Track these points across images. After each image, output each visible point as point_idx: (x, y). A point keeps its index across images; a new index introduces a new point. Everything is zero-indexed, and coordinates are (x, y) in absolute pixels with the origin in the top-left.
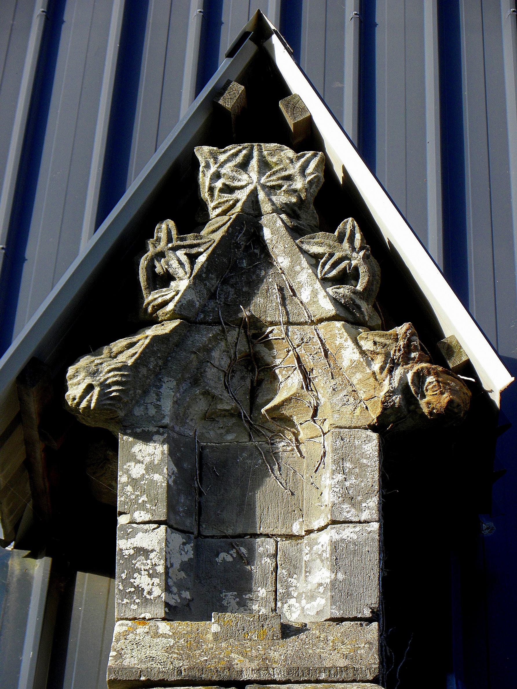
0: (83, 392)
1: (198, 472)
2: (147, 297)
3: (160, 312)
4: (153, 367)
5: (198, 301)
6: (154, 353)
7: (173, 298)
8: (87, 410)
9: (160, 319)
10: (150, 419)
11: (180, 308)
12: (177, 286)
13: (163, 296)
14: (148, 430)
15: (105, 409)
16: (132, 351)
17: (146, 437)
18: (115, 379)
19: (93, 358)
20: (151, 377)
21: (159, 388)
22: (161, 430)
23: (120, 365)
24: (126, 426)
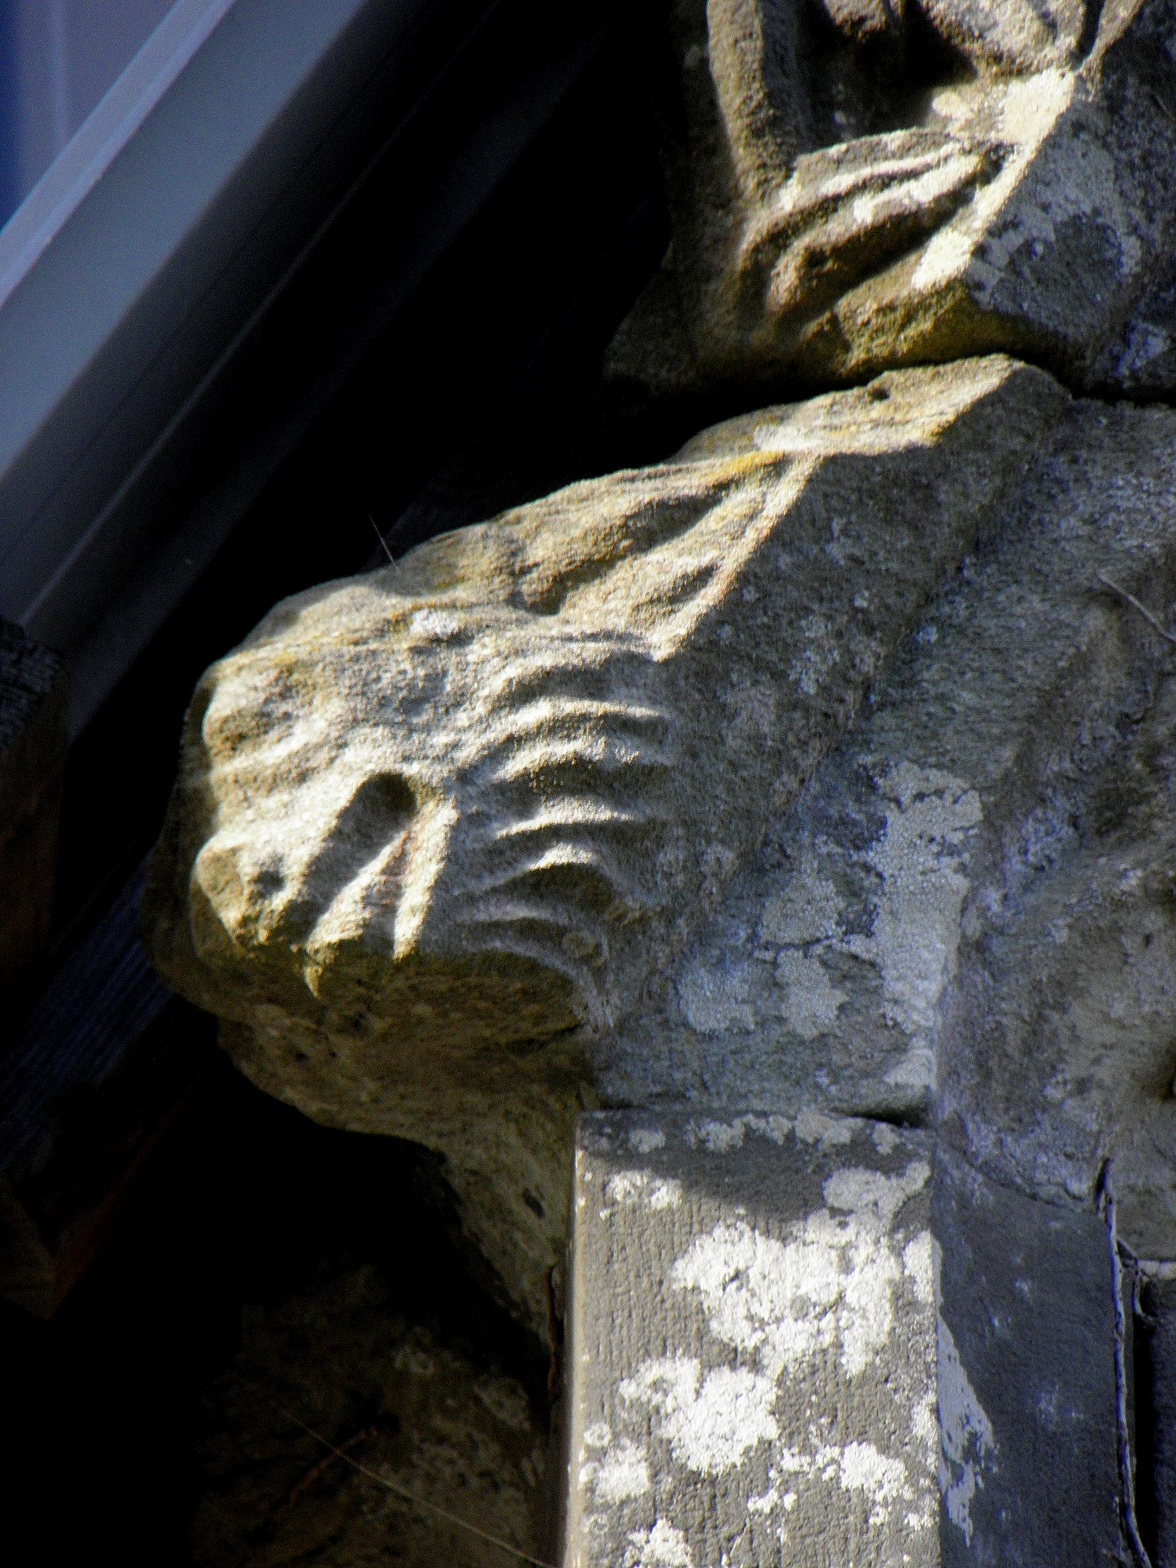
0: (336, 835)
1: (1130, 1464)
2: (766, 191)
3: (861, 304)
4: (824, 689)
5: (1134, 230)
6: (828, 585)
7: (955, 201)
8: (360, 970)
9: (857, 356)
10: (803, 1062)
11: (1013, 266)
12: (987, 118)
13: (887, 181)
14: (791, 1137)
15: (490, 959)
16: (670, 560)
17: (776, 1186)
18: (562, 750)
19: (393, 605)
20: (808, 762)
21: (862, 843)
22: (885, 1136)
23: (593, 652)
24: (625, 1105)
